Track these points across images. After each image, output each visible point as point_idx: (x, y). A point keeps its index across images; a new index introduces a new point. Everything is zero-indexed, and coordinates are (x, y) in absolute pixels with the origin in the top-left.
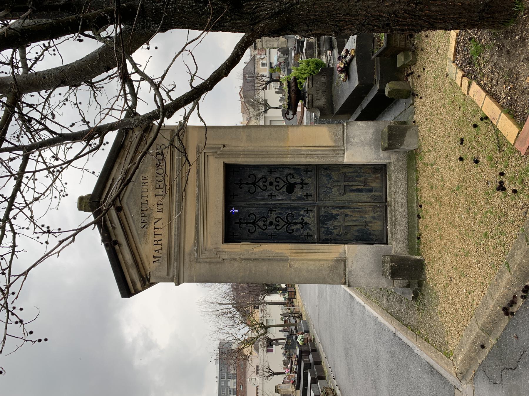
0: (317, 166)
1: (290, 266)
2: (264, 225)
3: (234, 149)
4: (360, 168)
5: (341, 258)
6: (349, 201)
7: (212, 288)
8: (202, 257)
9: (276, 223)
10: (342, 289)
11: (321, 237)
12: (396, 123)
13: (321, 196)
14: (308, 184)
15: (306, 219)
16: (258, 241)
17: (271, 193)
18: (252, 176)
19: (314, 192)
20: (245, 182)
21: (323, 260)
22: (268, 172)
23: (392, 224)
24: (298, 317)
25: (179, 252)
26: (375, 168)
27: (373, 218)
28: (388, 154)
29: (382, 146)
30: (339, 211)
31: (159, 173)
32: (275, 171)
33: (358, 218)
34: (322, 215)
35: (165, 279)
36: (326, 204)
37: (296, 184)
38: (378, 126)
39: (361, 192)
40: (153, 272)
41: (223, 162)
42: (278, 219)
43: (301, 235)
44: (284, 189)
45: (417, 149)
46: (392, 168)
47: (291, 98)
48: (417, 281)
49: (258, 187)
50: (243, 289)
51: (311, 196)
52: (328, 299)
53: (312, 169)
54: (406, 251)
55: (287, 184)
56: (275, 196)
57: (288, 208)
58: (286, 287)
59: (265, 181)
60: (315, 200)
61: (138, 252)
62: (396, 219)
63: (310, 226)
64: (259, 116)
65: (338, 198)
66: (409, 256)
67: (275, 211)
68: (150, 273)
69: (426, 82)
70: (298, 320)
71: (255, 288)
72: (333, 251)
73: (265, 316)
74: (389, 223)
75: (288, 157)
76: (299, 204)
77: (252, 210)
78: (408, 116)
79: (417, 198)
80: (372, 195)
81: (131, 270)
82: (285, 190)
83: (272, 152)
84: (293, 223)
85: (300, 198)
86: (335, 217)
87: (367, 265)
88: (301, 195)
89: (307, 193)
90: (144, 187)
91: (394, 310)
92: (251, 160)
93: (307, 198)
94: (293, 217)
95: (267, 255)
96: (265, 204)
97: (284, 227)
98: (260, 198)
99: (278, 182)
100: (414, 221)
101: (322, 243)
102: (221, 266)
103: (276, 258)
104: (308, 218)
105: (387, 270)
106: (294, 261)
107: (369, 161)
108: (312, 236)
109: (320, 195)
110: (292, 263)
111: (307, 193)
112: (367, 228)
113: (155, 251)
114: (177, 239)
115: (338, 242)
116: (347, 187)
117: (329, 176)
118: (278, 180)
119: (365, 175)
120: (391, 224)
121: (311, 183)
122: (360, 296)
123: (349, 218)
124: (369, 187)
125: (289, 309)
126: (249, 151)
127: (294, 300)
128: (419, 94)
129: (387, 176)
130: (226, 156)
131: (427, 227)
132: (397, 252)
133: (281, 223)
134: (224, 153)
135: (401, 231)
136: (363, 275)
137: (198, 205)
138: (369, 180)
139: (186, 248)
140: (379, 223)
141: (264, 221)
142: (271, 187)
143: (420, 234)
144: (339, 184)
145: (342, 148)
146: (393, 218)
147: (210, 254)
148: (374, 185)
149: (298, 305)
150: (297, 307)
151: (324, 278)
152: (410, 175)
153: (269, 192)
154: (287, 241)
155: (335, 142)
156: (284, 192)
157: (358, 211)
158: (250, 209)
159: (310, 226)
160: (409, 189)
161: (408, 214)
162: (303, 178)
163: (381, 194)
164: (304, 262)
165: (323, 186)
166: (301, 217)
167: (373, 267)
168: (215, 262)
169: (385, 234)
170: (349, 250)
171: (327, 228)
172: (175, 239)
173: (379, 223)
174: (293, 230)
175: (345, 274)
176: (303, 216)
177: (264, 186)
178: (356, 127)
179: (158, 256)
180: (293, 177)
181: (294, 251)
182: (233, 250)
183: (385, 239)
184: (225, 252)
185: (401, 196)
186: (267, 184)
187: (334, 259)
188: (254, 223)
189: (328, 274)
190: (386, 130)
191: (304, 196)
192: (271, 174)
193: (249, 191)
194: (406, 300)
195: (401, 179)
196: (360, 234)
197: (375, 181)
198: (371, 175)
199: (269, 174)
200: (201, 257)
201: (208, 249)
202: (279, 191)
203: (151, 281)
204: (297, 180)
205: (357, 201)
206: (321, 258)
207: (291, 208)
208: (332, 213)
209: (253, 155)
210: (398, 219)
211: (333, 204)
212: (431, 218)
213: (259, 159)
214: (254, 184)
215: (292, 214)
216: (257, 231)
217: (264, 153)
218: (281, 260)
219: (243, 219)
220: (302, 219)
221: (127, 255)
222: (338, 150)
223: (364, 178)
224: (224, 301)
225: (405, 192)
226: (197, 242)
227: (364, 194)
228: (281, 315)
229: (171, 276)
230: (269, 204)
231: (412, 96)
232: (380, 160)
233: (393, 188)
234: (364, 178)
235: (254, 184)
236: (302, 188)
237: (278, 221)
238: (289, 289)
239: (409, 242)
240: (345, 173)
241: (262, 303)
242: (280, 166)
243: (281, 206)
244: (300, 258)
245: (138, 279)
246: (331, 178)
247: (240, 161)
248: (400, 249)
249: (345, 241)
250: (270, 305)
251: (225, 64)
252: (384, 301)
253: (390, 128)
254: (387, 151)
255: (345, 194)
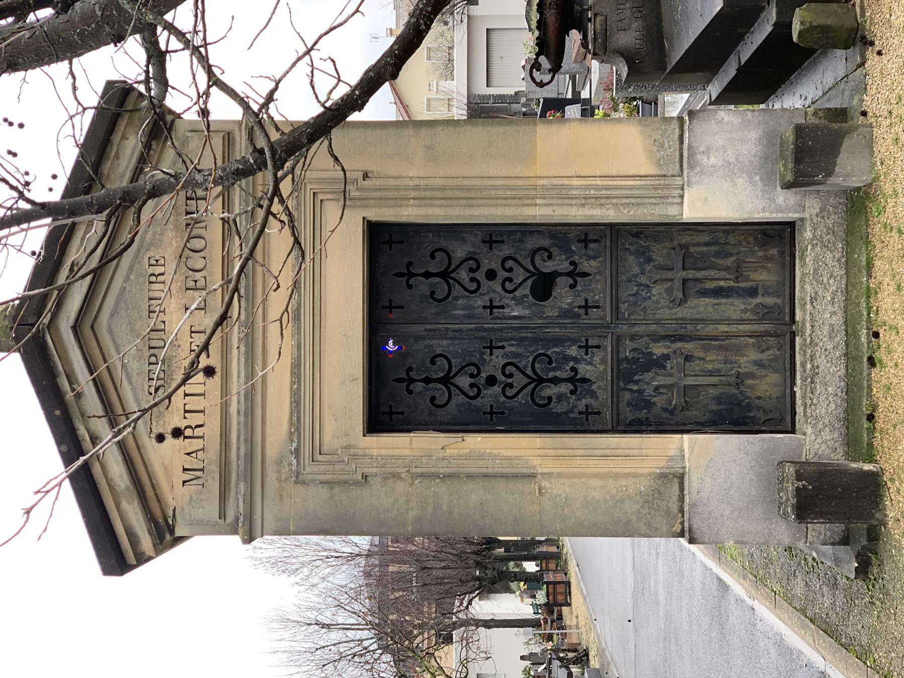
0: (612, 226)
1: (540, 492)
2: (472, 386)
3: (392, 182)
4: (724, 231)
5: (672, 471)
6: (695, 321)
7: (301, 576)
8: (309, 469)
9: (504, 379)
10: (698, 564)
12: (821, 114)
13: (623, 307)
14: (589, 275)
15: (584, 370)
16: (457, 428)
17: (491, 301)
20: (422, 271)
21: (626, 476)
22: (484, 242)
23: (806, 380)
24: (577, 661)
25: (250, 458)
27: (759, 364)
29: (782, 177)
30: (669, 347)
31: (193, 248)
32: (502, 242)
33: (717, 366)
34: (626, 358)
35: (214, 526)
36: (637, 328)
37: (555, 275)
38: (772, 123)
39: (727, 296)
40: (183, 509)
41: (364, 218)
42: (510, 369)
43: (571, 411)
44: (525, 290)
45: (870, 185)
46: (808, 234)
47: (546, 24)
48: (865, 526)
50: (402, 579)
51: (598, 307)
52: (661, 598)
54: (840, 450)
55: (533, 274)
56: (502, 307)
57: (535, 340)
58: (541, 570)
60: (608, 318)
61: (142, 457)
62: (815, 368)
63: (594, 387)
64: (452, 14)
65: (666, 313)
66: (846, 462)
67: (503, 347)
68: (174, 510)
69: (891, 16)
70: (575, 670)
71: (441, 573)
72: (651, 452)
73: (473, 656)
74: (798, 377)
75: (536, 205)
76: (566, 328)
77: (441, 345)
78: (852, 97)
79: (869, 314)
80: (757, 305)
81: (124, 504)
82: (527, 291)
83: (488, 192)
85: (568, 313)
86: (659, 363)
87: (739, 487)
89: (586, 300)
90: (155, 287)
91: (820, 609)
93: (586, 314)
94: (550, 363)
95: (481, 463)
96: (476, 329)
97: (525, 391)
100: (861, 374)
101: (625, 432)
102: (359, 492)
104: (589, 367)
105: (788, 500)
106: (550, 478)
107: (746, 216)
108: (599, 413)
109: (620, 305)
110: (545, 483)
111: (586, 300)
113: (188, 454)
114: (246, 423)
115: (667, 428)
116: (690, 284)
117: (645, 256)
118: (510, 264)
120: (804, 380)
122: (741, 581)
123: (696, 366)
125: (550, 638)
127: (565, 609)
128: (877, 42)
130: (372, 202)
131: (889, 389)
132: (816, 454)
133: (519, 380)
135: (827, 399)
136: (727, 513)
137: (299, 333)
139: (268, 446)
140: (773, 378)
141: (472, 376)
142: (491, 283)
143: (875, 408)
144: (669, 275)
145: (678, 181)
146: (809, 366)
147: (330, 463)
148: (762, 278)
149: (577, 627)
150: (574, 631)
151: (629, 522)
152: (854, 252)
153: (487, 298)
155: (659, 165)
156: (526, 296)
157: (720, 347)
158: (435, 342)
159: (594, 387)
160: (850, 288)
161: (846, 355)
162: (576, 258)
163: (779, 301)
164: (576, 480)
165: (629, 281)
166: (571, 364)
167: (754, 492)
168: (346, 482)
170: (692, 449)
171: (638, 391)
172: (239, 423)
173: (773, 378)
174: (550, 399)
175: (682, 511)
176: (576, 360)
177: (472, 280)
178: (713, 126)
179: (195, 467)
180: (550, 257)
181: (552, 452)
182: (390, 452)
184: (371, 457)
185: (830, 307)
186: (480, 275)
187: (654, 473)
188: (446, 381)
189: (638, 511)
190: (790, 135)
191: (579, 307)
192: (491, 248)
193: (432, 293)
194: (845, 580)
195: (831, 263)
196: (722, 407)
198: (753, 252)
199: (485, 249)
200: (308, 470)
201: (325, 449)
203: (178, 533)
204: (560, 264)
205: (716, 320)
206: (620, 470)
208: (651, 354)
210: (822, 368)
211: (653, 327)
212: (896, 365)
214: (445, 275)
216: (454, 401)
217: (473, 194)
218: (516, 476)
220: (573, 369)
221: (115, 465)
222: (667, 187)
224: (342, 618)
225: (840, 297)
226: (298, 429)
228: (523, 658)
229: (230, 517)
230: (485, 330)
231: (859, 44)
232: (777, 212)
233: (808, 287)
234: (734, 258)
235: (445, 275)
236: (572, 287)
237: (511, 376)
238: (550, 577)
239: (847, 428)
240: (684, 247)
241: (466, 623)
242: (515, 228)
243: (518, 335)
244: (565, 470)
245: (145, 529)
246: (649, 260)
247: (409, 214)
248: (823, 447)
250: (489, 627)
251: (390, 53)
252: (799, 589)
253: (799, 130)
255: (686, 302)
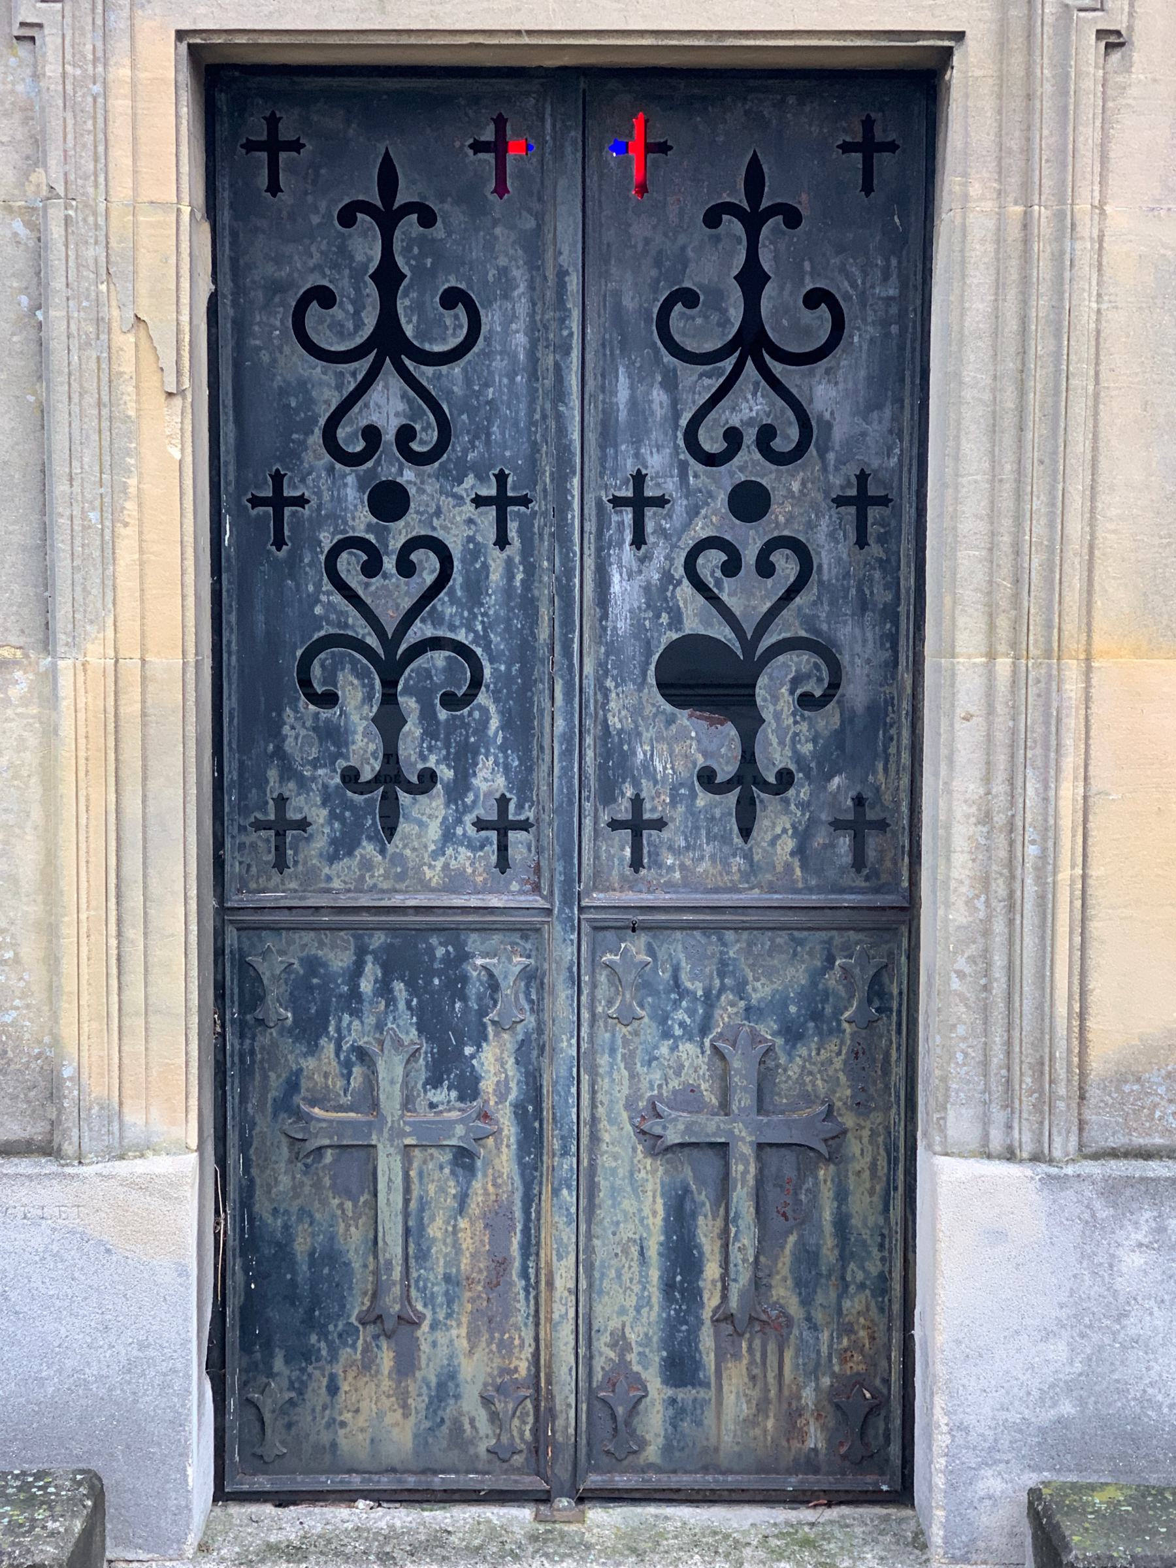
2: (372, 434)
3: (1088, 135)
5: (69, 1120)
11: (270, 942)
13: (636, 947)
14: (746, 832)
17: (661, 502)
18: (820, 321)
19: (670, 886)
21: (52, 961)
22: (862, 478)
26: (878, 1407)
28: (998, 1542)
30: (502, 1097)
32: (862, 542)
33: (439, 1252)
34: (464, 956)
36: (564, 994)
39: (669, 1287)
41: (959, 36)
42: (428, 565)
43: (288, 771)
49: (716, 383)
51: (636, 863)
53: (875, 874)
55: (749, 646)
56: (639, 540)
57: (524, 652)
59: (779, 445)
60: (599, 898)
63: (368, 849)
67: (502, 541)
74: (401, 1517)
75: (991, 655)
76: (567, 753)
80: (638, 1382)
82: (692, 625)
84: (389, 698)
88: (648, 769)
89: (660, 824)
92: (978, 307)
93: (615, 825)
94: (450, 701)
95: (88, 457)
97: (354, 617)
98: (623, 395)
99: (765, 568)
103: (62, 543)
104: (434, 831)
107: (940, 1369)
108: (281, 864)
109: (643, 939)
111: (660, 824)
112: (350, 1330)
115: (233, 1090)
116: (710, 1163)
118: (786, 566)
119: (814, 1328)
121: (748, 856)
124: (709, 1360)
126: (1059, 281)
129: (806, 1514)
130: (1017, 61)
134: (1047, 40)
138: (772, 1359)
141: (406, 434)
142: (721, 500)
144: (743, 1100)
145: (1063, 1144)
148: (730, 1399)
153: (670, 486)
154: (231, 637)
155: (1121, 1079)
156: (676, 620)
159: (368, 849)
162: (801, 791)
163: (652, 1453)
164: (35, 790)
165: (723, 969)
166: (446, 773)
169: (303, 1482)
170: (145, 1185)
171: (355, 994)
174: (329, 699)
176: (459, 790)
177: (733, 437)
180: (806, 701)
181: (131, 708)
182: (120, 129)
183: (263, 1482)
184: (103, 58)
191: (637, 802)
192: (840, 501)
193: (689, 298)
197: (762, 1407)
198: (814, 1372)
199: (837, 481)
202: (679, 572)
205: (590, 1250)
207: (529, 684)
208: (480, 1038)
209: (1024, 321)
211: (567, 1047)
213: (986, 379)
215: (470, 696)
216: (317, 370)
217: (1037, 431)
219: (422, 241)
220: (428, 779)
222: (1045, 1104)
223: (794, 1308)
227: (654, 1313)
230: (560, 480)
232: (949, 1472)
234: (794, 1308)
236: (707, 778)
242: (907, 581)
243: (544, 591)
244: (66, 753)
246: (792, 1034)
249: (245, 1145)
254: (1026, 1530)
